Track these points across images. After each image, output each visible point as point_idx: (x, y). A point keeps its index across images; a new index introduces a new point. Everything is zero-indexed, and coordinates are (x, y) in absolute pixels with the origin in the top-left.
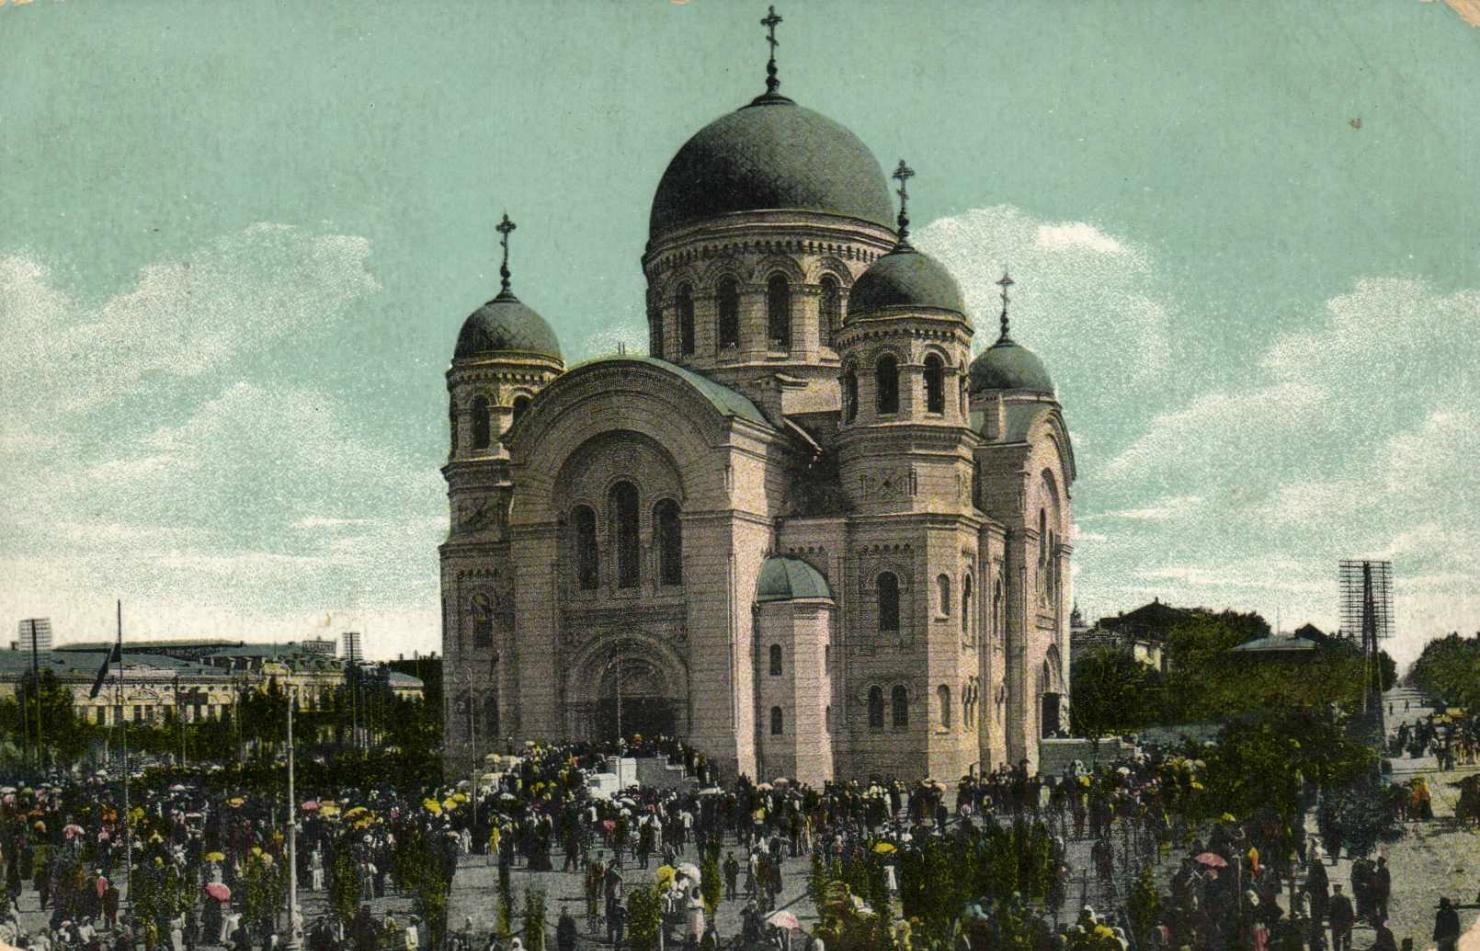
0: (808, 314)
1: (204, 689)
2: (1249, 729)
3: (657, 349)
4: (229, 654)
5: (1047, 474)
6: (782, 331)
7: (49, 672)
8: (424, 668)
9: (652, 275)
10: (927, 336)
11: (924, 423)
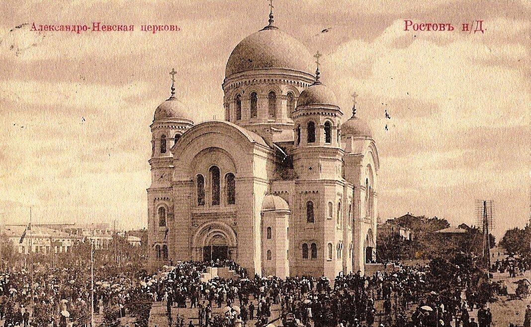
0: (283, 106)
5: (369, 166)
6: (273, 113)
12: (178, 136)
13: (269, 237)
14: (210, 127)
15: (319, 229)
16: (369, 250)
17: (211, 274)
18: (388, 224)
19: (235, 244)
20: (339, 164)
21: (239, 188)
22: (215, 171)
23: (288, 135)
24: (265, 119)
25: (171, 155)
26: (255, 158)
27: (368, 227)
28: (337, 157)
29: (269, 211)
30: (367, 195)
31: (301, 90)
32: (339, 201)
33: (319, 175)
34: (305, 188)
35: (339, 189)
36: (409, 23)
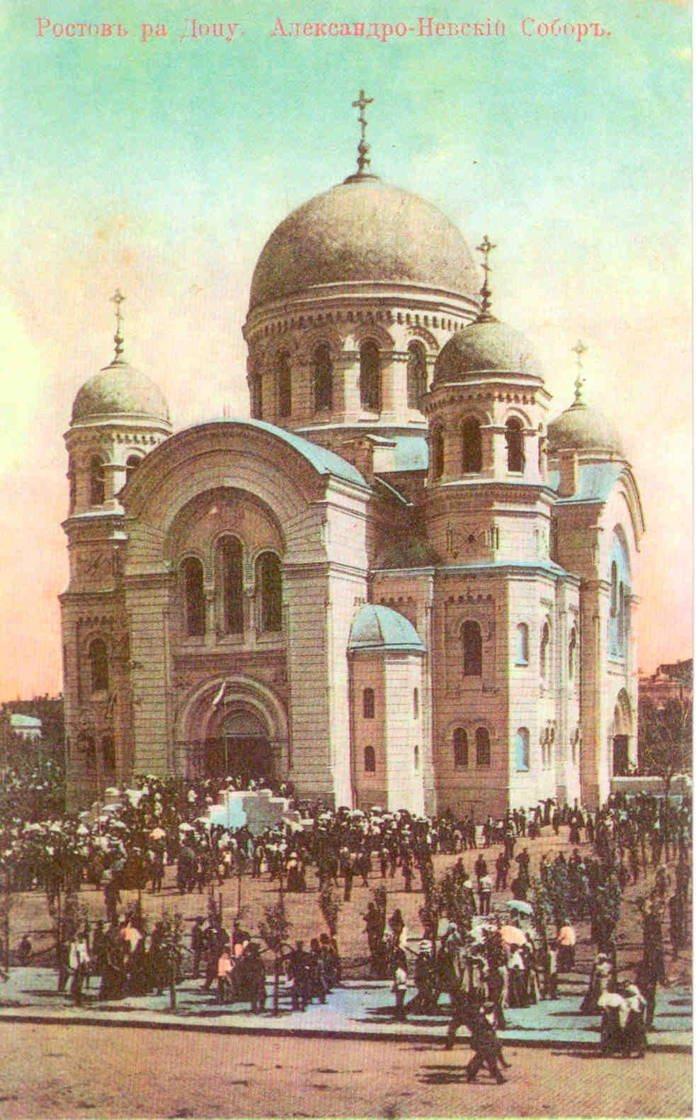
0: (397, 377)
3: (257, 413)
5: (618, 529)
6: (373, 397)
12: (133, 460)
13: (369, 713)
14: (211, 438)
15: (498, 692)
16: (620, 744)
17: (230, 810)
18: (662, 676)
19: (284, 734)
20: (545, 526)
21: (289, 591)
22: (231, 549)
23: (411, 453)
24: (354, 412)
25: (119, 510)
26: (330, 512)
28: (540, 507)
29: (369, 655)
30: (614, 603)
31: (443, 337)
32: (546, 620)
33: (492, 555)
34: (460, 589)
35: (544, 588)
36: (44, 23)
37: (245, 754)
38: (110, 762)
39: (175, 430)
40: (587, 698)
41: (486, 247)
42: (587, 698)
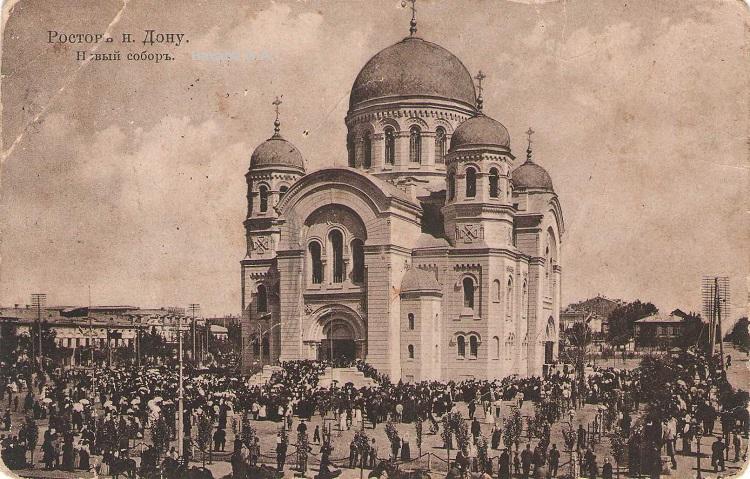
0: (429, 145)
1: (119, 331)
2: (657, 365)
3: (352, 161)
4: (133, 313)
5: (550, 230)
6: (416, 154)
7: (46, 321)
8: (234, 327)
9: (350, 127)
10: (466, 160)
11: (466, 203)
12: (283, 189)
16: (549, 346)
24: (404, 163)
27: (548, 314)
37: (344, 347)
38: (266, 352)
39: (307, 173)
40: (531, 318)
41: (481, 77)
42: (531, 318)
